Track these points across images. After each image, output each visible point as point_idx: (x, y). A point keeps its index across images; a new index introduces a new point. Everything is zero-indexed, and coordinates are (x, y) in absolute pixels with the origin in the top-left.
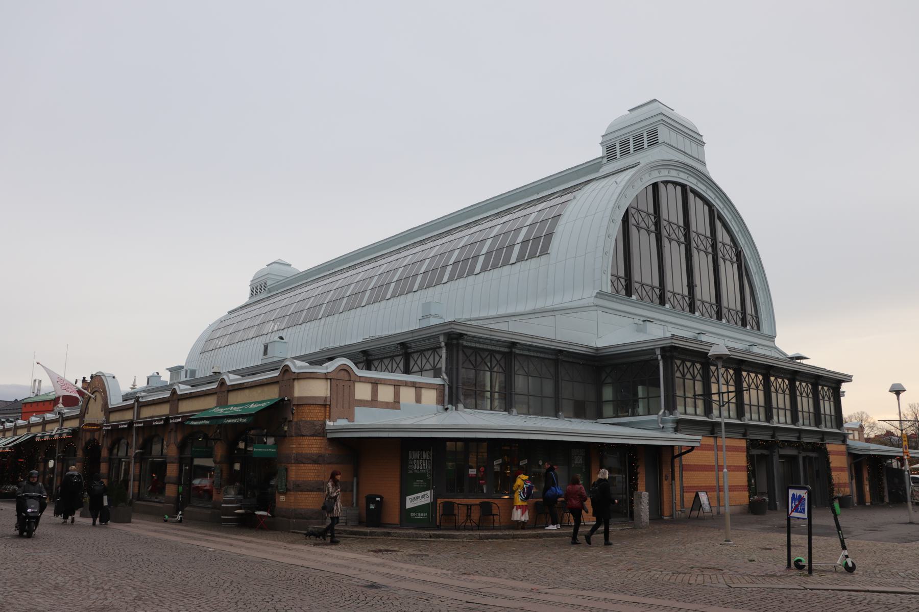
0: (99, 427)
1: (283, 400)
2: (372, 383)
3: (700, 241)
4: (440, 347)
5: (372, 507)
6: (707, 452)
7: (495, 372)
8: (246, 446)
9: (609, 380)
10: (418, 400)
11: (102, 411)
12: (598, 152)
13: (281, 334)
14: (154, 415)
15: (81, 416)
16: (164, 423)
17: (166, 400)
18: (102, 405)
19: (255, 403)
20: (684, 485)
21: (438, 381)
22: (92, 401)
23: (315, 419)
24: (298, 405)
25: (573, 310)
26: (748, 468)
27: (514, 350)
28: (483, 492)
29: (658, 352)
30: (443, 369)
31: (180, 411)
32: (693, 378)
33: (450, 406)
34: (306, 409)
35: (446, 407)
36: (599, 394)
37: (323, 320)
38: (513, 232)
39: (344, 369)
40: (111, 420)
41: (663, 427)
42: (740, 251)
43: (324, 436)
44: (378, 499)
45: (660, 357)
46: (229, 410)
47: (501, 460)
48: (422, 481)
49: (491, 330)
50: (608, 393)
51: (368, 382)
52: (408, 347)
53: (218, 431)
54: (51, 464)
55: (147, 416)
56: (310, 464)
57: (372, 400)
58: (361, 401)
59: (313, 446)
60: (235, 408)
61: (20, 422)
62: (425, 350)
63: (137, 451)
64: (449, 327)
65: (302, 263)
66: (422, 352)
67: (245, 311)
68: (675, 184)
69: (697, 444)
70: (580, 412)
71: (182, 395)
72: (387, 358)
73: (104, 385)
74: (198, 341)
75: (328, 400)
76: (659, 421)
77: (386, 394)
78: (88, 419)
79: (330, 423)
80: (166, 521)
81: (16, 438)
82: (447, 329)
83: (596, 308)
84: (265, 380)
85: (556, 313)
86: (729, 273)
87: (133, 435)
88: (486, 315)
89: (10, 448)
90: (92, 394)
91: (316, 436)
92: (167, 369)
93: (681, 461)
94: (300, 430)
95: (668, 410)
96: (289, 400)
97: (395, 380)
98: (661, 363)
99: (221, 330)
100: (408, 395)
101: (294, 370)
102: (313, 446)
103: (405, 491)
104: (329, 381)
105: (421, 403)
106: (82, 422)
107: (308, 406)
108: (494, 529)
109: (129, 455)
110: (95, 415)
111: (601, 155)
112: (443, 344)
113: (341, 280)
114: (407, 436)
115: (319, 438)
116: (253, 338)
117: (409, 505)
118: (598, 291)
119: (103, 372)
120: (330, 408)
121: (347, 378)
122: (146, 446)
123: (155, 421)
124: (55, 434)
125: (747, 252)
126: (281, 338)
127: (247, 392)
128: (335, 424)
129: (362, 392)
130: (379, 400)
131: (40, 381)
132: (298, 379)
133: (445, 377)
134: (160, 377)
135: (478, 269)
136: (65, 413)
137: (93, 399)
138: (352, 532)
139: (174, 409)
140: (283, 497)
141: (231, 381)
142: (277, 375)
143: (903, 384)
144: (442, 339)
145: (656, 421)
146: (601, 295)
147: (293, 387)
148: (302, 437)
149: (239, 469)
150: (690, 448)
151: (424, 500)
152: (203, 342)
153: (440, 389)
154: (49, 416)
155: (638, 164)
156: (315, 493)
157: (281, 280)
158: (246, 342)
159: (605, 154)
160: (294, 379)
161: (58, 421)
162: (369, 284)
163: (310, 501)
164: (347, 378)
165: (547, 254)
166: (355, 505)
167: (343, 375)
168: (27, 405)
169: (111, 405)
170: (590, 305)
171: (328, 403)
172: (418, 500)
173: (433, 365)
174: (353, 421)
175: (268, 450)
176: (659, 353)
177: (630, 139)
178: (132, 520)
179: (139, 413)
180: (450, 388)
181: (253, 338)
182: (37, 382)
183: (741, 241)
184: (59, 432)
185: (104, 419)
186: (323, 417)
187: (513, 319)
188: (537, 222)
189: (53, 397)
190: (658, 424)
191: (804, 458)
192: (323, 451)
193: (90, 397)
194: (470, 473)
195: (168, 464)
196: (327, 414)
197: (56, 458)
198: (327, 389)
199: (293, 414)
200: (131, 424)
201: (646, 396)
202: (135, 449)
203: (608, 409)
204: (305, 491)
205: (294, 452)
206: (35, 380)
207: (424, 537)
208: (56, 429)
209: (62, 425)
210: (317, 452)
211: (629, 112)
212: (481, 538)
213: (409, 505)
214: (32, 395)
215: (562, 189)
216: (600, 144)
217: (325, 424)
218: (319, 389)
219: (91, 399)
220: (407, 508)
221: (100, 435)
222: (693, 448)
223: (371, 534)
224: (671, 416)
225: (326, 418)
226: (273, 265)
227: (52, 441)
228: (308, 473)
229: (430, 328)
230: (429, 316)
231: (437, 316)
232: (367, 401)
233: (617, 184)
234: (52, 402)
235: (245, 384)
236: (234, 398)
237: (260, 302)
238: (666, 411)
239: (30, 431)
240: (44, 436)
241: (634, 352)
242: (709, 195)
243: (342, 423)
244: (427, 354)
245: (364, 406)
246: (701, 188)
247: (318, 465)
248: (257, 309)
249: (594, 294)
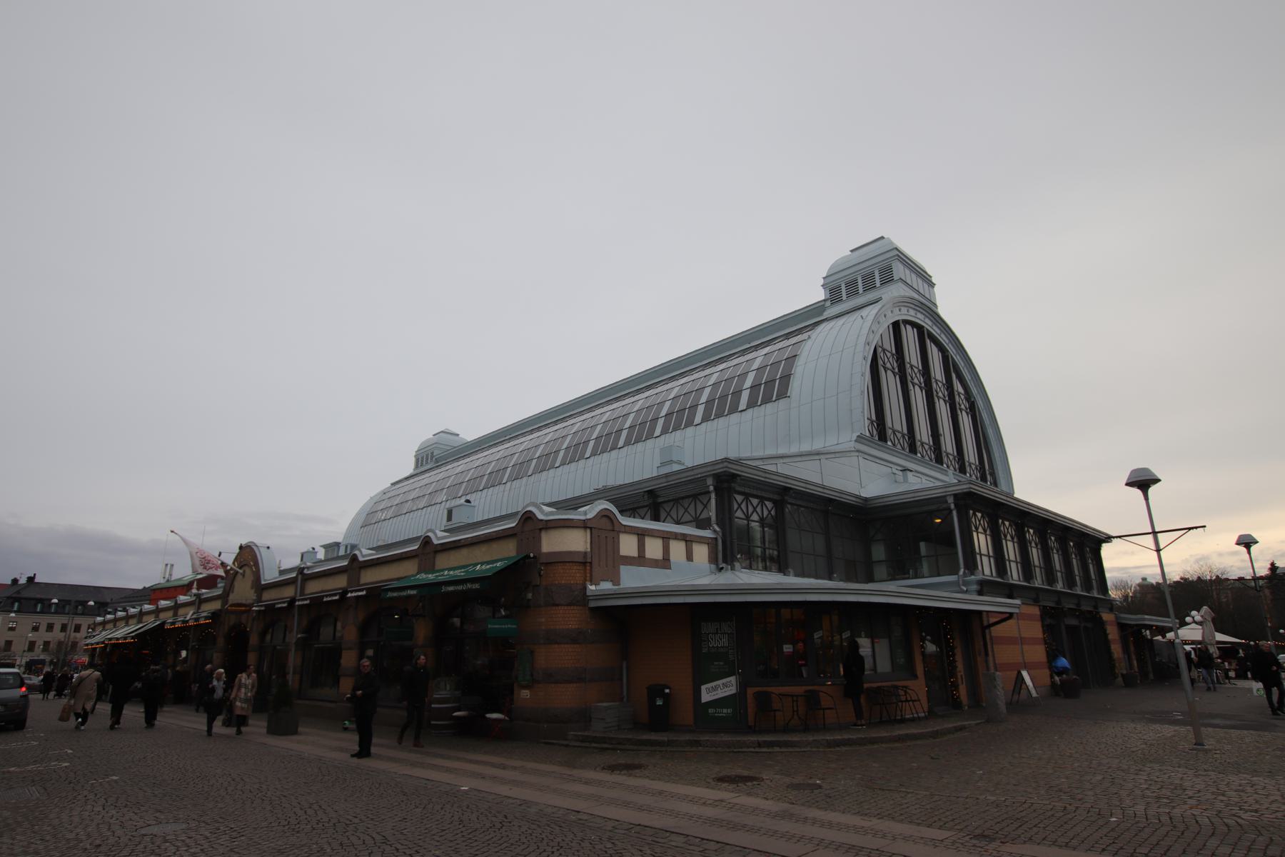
1: (528, 557)
2: (638, 534)
3: (940, 389)
4: (709, 492)
5: (659, 702)
8: (462, 623)
10: (690, 557)
12: (819, 295)
13: (468, 497)
14: (324, 589)
16: (311, 602)
18: (253, 581)
19: (482, 564)
20: (997, 662)
21: (707, 533)
22: (239, 577)
23: (572, 582)
24: (547, 564)
25: (837, 455)
26: (1045, 641)
27: (786, 498)
28: (802, 676)
29: (951, 500)
30: (714, 519)
31: (362, 581)
33: (724, 565)
35: (721, 566)
36: (868, 554)
37: (509, 484)
38: (694, 393)
39: (605, 515)
40: (264, 599)
41: (967, 590)
42: (973, 402)
44: (667, 691)
45: (952, 506)
46: (443, 575)
47: (849, 632)
48: (722, 663)
49: (765, 471)
51: (634, 534)
53: (421, 604)
54: (184, 654)
55: (314, 591)
56: (567, 643)
58: (626, 557)
59: (569, 619)
60: (451, 573)
61: (147, 607)
62: (683, 498)
63: (299, 636)
64: (721, 466)
65: (470, 434)
66: (677, 501)
67: (412, 481)
69: (1016, 611)
71: (365, 561)
72: (688, 497)
73: (256, 556)
74: (358, 514)
75: (589, 556)
76: (961, 582)
77: (654, 549)
78: (233, 598)
79: (593, 587)
80: (346, 729)
81: (141, 625)
82: (719, 469)
83: (857, 454)
84: (494, 534)
85: (822, 457)
86: (965, 421)
87: (294, 616)
88: (775, 453)
89: (133, 638)
90: (240, 568)
92: (321, 546)
93: (990, 633)
95: (968, 569)
96: (534, 557)
97: (663, 531)
98: (955, 513)
99: (384, 502)
100: (677, 549)
102: (569, 619)
103: (701, 677)
104: (588, 531)
105: (692, 561)
107: (562, 564)
109: (287, 640)
110: (243, 592)
111: (823, 298)
112: (711, 488)
113: (526, 442)
114: (744, 600)
115: (578, 608)
116: (407, 513)
117: (706, 697)
118: (859, 434)
119: (255, 541)
121: (610, 528)
122: (312, 630)
123: (327, 596)
124: (190, 619)
125: (980, 403)
126: (468, 501)
127: (465, 551)
128: (598, 588)
129: (628, 545)
131: (172, 565)
133: (718, 529)
134: (316, 553)
135: (698, 419)
136: (203, 594)
137: (241, 574)
139: (354, 582)
140: (527, 691)
143: (1253, 535)
144: (710, 481)
145: (956, 583)
146: (860, 439)
148: (554, 608)
150: (1008, 615)
151: (726, 689)
152: (365, 515)
153: (712, 543)
154: (182, 598)
155: (880, 299)
156: (575, 685)
157: (448, 450)
158: (416, 512)
159: (828, 296)
160: (541, 530)
162: (562, 443)
163: (565, 697)
164: (610, 528)
165: (786, 397)
166: (625, 700)
169: (265, 580)
170: (851, 449)
171: (589, 560)
172: (719, 689)
173: (694, 516)
174: (619, 585)
175: (506, 626)
176: (953, 501)
177: (859, 283)
178: (300, 729)
179: (303, 588)
180: (724, 543)
181: (407, 513)
182: (169, 566)
183: (974, 391)
184: (195, 616)
185: (255, 598)
186: (582, 578)
187: (781, 461)
188: (768, 365)
189: (186, 582)
190: (959, 586)
193: (237, 572)
194: (785, 650)
195: (343, 651)
196: (588, 575)
197: (190, 647)
198: (586, 542)
199: (540, 575)
200: (292, 602)
202: (297, 634)
203: (880, 571)
204: (560, 683)
205: (543, 628)
206: (167, 565)
207: (751, 747)
208: (191, 612)
209: (199, 608)
210: (577, 626)
211: (850, 253)
212: (830, 744)
213: (706, 697)
214: (162, 581)
215: (786, 332)
216: (822, 286)
217: (585, 588)
218: (576, 542)
219: (239, 574)
220: (703, 702)
223: (670, 743)
224: (973, 577)
225: (586, 580)
227: (186, 628)
228: (563, 657)
229: (693, 470)
230: (671, 462)
231: (679, 463)
232: (634, 557)
233: (862, 316)
234: (185, 587)
235: (463, 541)
236: (442, 561)
238: (967, 571)
240: (175, 622)
241: (905, 503)
242: (943, 339)
243: (606, 586)
244: (686, 503)
245: (631, 565)
246: (935, 331)
247: (578, 646)
248: (426, 478)
249: (854, 438)
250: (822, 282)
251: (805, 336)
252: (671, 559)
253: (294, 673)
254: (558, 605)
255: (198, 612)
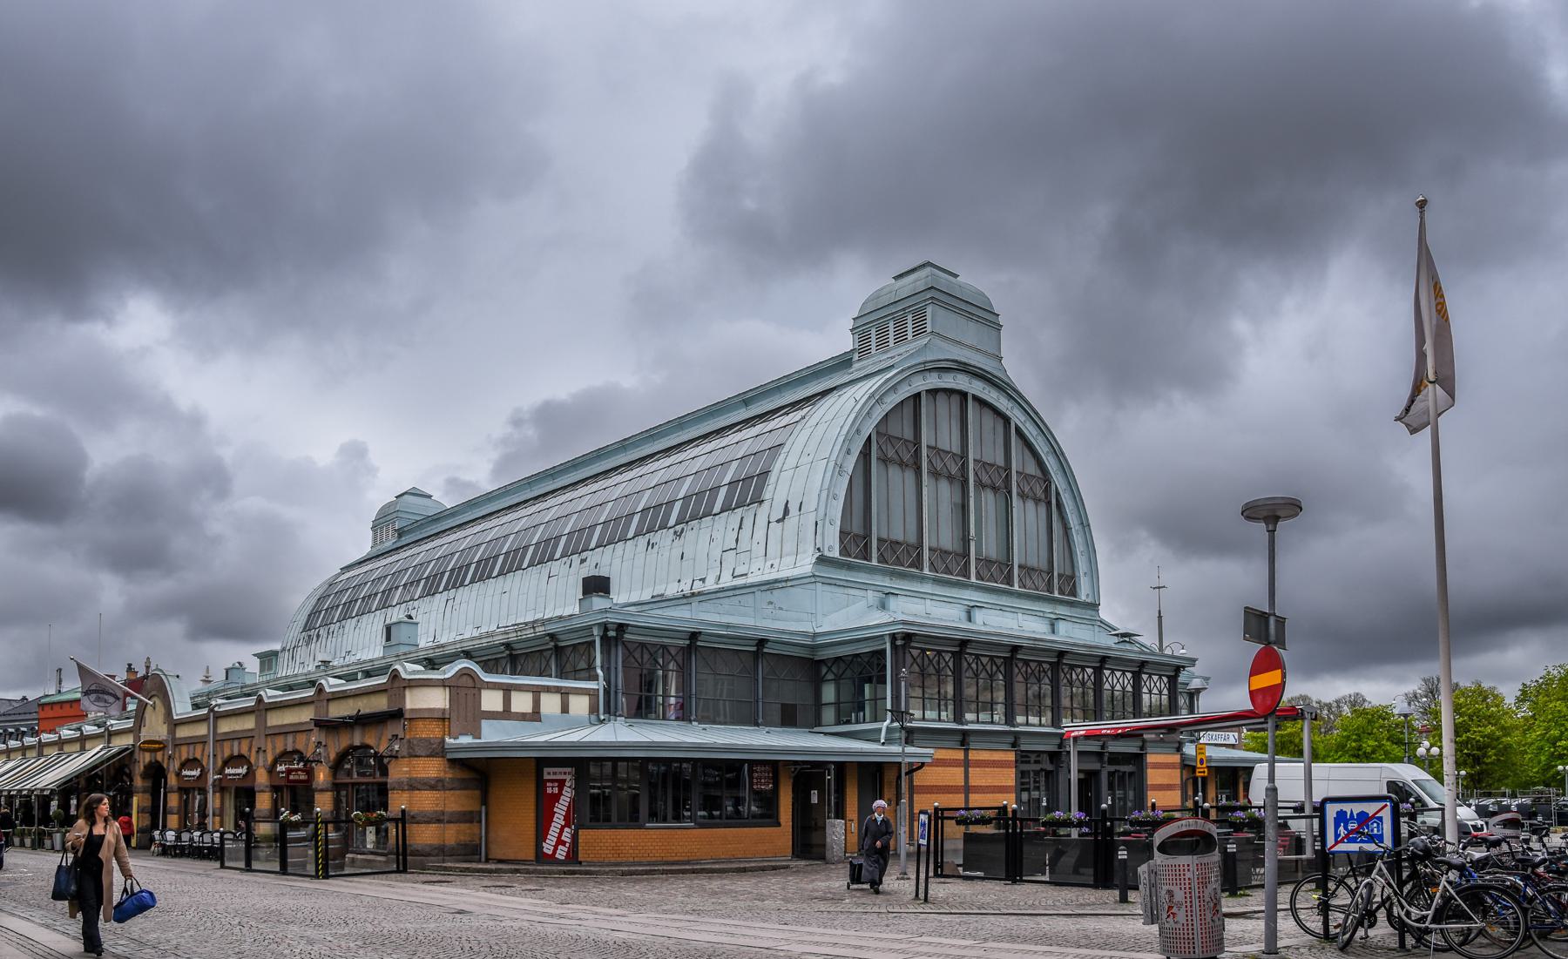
0: (161, 746)
6: (951, 768)
7: (670, 670)
9: (830, 676)
10: (565, 709)
11: (165, 723)
15: (136, 730)
17: (250, 709)
22: (149, 709)
32: (921, 671)
34: (420, 724)
36: (818, 694)
43: (443, 757)
50: (829, 693)
52: (558, 640)
57: (504, 711)
63: (215, 777)
68: (950, 392)
69: (929, 760)
70: (789, 718)
71: (269, 703)
77: (522, 703)
79: (452, 741)
91: (433, 756)
94: (414, 750)
100: (550, 704)
101: (404, 675)
104: (448, 689)
106: (137, 738)
108: (481, 844)
120: (449, 722)
129: (491, 701)
130: (513, 710)
132: (410, 687)
138: (475, 869)
141: (331, 687)
142: (385, 681)
147: (404, 697)
149: (816, 802)
153: (592, 694)
156: (434, 825)
160: (405, 687)
161: (104, 736)
164: (471, 684)
167: (466, 681)
168: (46, 708)
169: (177, 715)
191: (1111, 774)
192: (442, 775)
196: (446, 730)
201: (873, 698)
203: (829, 714)
209: (109, 742)
216: (851, 330)
217: (444, 741)
218: (436, 700)
219: (149, 706)
221: (163, 755)
222: (923, 764)
226: (406, 496)
232: (497, 712)
237: (385, 556)
239: (62, 750)
243: (465, 740)
250: (851, 325)
251: (796, 416)
252: (541, 711)
253: (214, 815)
254: (419, 757)
255: (109, 747)
